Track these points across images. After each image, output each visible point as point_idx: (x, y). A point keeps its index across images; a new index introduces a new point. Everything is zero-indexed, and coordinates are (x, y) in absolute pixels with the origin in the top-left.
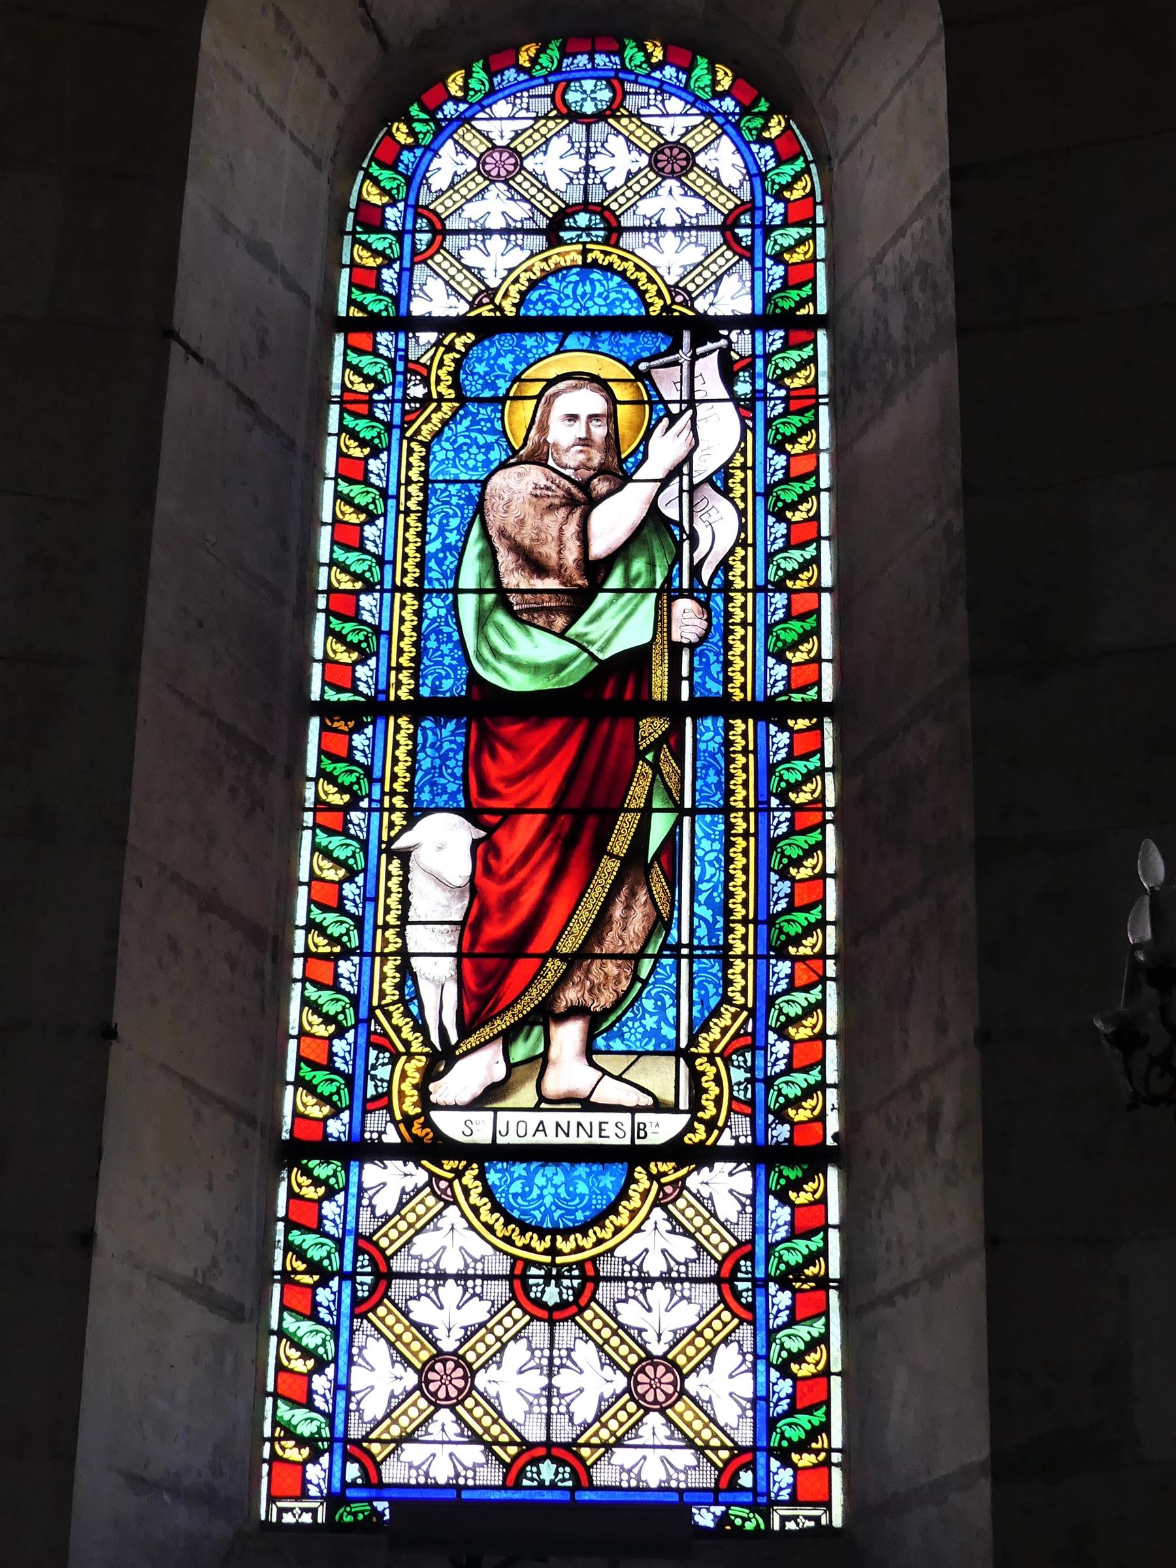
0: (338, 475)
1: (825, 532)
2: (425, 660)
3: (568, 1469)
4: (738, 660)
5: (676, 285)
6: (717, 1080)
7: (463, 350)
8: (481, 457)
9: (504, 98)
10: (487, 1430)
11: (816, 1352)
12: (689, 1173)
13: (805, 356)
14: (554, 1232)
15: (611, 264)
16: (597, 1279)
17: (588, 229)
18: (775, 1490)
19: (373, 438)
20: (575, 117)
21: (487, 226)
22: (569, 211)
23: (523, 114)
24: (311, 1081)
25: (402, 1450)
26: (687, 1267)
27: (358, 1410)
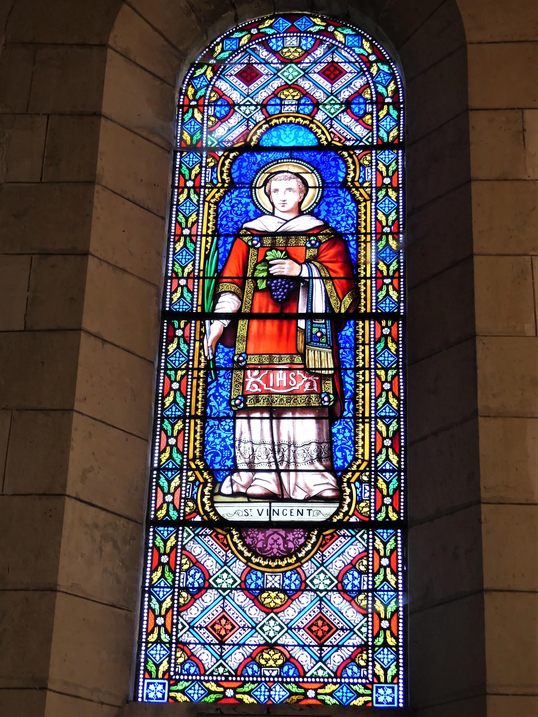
8: (243, 209)
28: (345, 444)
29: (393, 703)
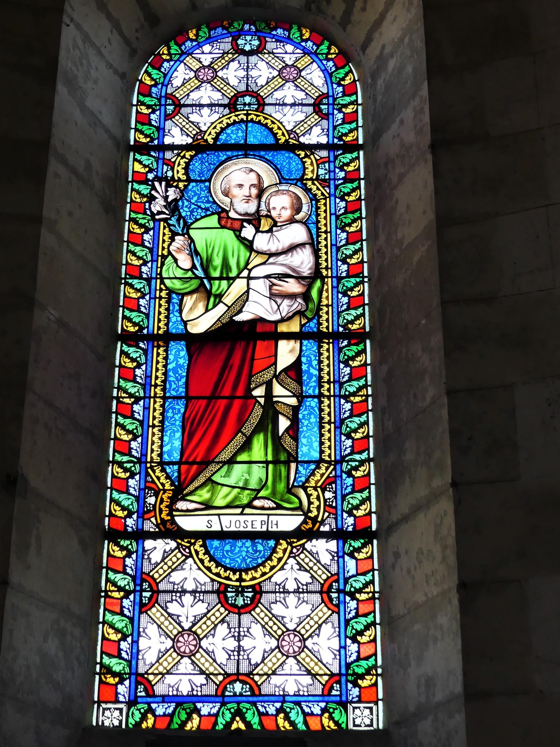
0: (128, 242)
1: (364, 237)
2: (166, 423)
3: (248, 686)
4: (325, 360)
5: (292, 130)
6: (318, 498)
7: (189, 158)
9: (209, 43)
10: (207, 669)
11: (369, 630)
12: (306, 542)
13: (354, 157)
14: (241, 571)
15: (260, 121)
16: (261, 593)
17: (250, 104)
18: (346, 526)
19: (140, 322)
20: (243, 52)
21: (201, 103)
22: (240, 95)
23: (217, 51)
24: (109, 665)
25: (165, 678)
26: (307, 586)
27: (143, 658)
28: (310, 430)
29: (371, 725)
